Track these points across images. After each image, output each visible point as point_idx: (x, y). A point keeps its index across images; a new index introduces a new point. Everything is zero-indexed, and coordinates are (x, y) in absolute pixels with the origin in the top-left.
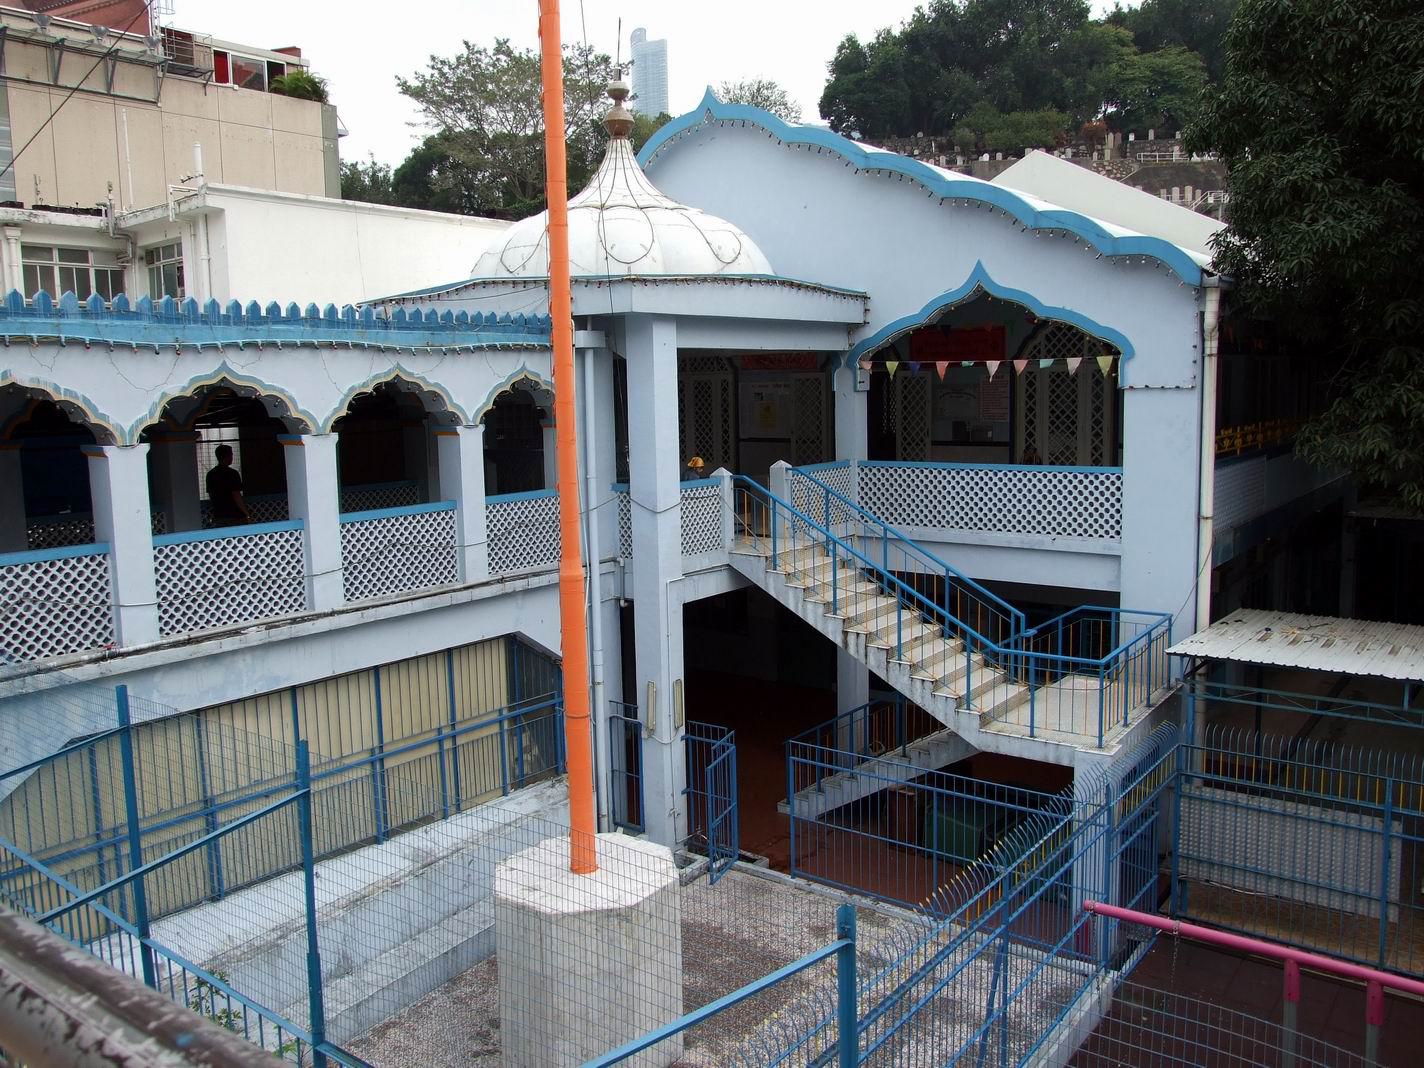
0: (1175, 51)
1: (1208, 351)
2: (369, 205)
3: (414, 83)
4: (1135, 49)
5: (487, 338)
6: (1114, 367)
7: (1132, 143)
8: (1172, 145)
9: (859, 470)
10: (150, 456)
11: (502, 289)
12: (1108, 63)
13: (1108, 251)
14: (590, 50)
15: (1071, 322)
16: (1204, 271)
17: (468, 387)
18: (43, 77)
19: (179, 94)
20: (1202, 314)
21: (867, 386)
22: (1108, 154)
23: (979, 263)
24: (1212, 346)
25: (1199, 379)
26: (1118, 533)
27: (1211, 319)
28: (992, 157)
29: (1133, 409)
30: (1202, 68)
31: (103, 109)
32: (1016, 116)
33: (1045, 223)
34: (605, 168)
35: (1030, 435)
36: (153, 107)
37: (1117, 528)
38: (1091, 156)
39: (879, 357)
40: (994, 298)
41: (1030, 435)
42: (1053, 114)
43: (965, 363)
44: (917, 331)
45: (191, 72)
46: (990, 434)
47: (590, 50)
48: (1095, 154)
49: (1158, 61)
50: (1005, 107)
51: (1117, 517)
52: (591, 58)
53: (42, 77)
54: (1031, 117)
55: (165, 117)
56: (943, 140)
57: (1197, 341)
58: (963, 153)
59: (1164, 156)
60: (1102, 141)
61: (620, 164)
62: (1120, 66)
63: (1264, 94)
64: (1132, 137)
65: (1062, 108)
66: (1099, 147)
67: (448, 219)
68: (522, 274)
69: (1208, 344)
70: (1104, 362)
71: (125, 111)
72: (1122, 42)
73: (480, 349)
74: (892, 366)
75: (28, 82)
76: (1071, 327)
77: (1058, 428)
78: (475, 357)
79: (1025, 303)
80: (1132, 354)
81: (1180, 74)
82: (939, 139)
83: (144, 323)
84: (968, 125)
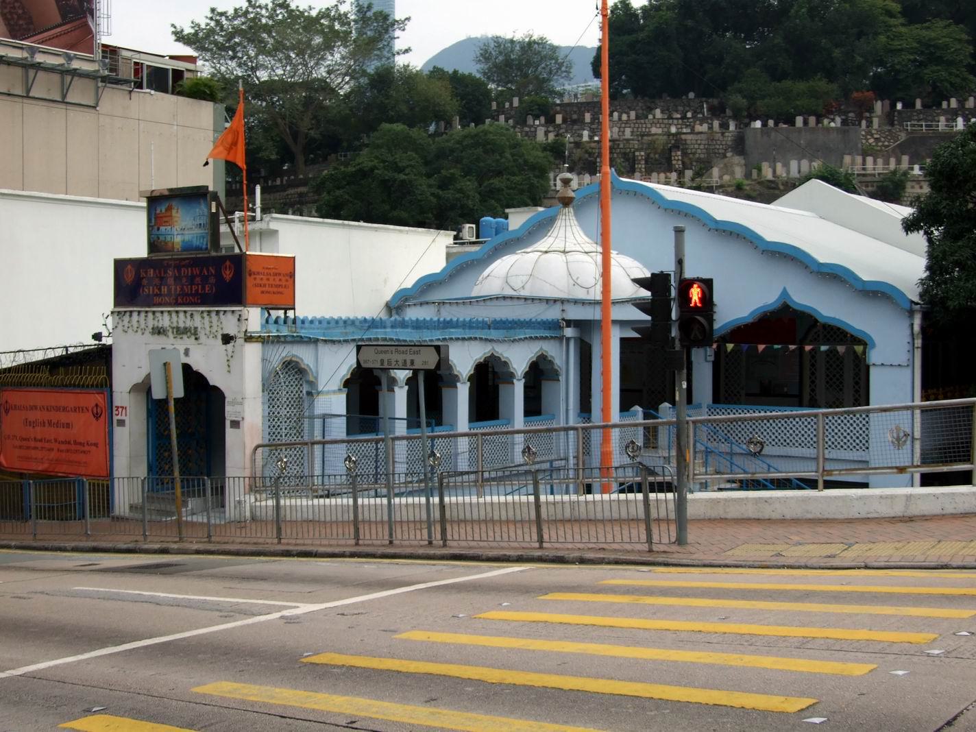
0: (941, 23)
1: (916, 345)
2: (340, 222)
3: (188, 30)
4: (902, 20)
5: (529, 333)
6: (864, 352)
7: (899, 111)
8: (938, 115)
9: (707, 410)
10: (408, 391)
11: (515, 302)
12: (876, 34)
13: (860, 287)
14: (369, 7)
15: (839, 325)
16: (912, 302)
17: (519, 358)
18: (19, 91)
19: (113, 100)
20: (912, 325)
21: (712, 359)
22: (876, 121)
23: (785, 288)
24: (918, 342)
25: (911, 360)
26: (867, 448)
27: (917, 328)
28: (765, 125)
29: (875, 376)
30: (968, 42)
31: (58, 112)
32: (787, 84)
33: (824, 270)
34: (559, 225)
35: (813, 390)
36: (93, 111)
37: (867, 445)
38: (860, 124)
39: (724, 339)
40: (794, 310)
41: (813, 390)
42: (821, 84)
43: (776, 346)
44: (746, 326)
45: (118, 82)
46: (786, 389)
47: (369, 7)
48: (864, 123)
49: (924, 33)
50: (777, 75)
51: (867, 445)
52: (369, 14)
53: (19, 91)
54: (801, 86)
55: (102, 118)
56: (715, 102)
57: (909, 339)
58: (735, 117)
59: (931, 126)
60: (871, 109)
61: (568, 223)
62: (888, 37)
63: (944, 207)
64: (899, 106)
65: (830, 76)
66: (867, 114)
67: (400, 231)
68: (524, 293)
69: (916, 341)
70: (859, 349)
71: (74, 113)
72: (890, 14)
73: (526, 338)
74: (730, 346)
75: (9, 95)
76: (839, 329)
77: (831, 386)
78: (522, 343)
79: (813, 314)
80: (874, 346)
81: (946, 46)
82: (710, 100)
83: (409, 330)
84: (740, 91)
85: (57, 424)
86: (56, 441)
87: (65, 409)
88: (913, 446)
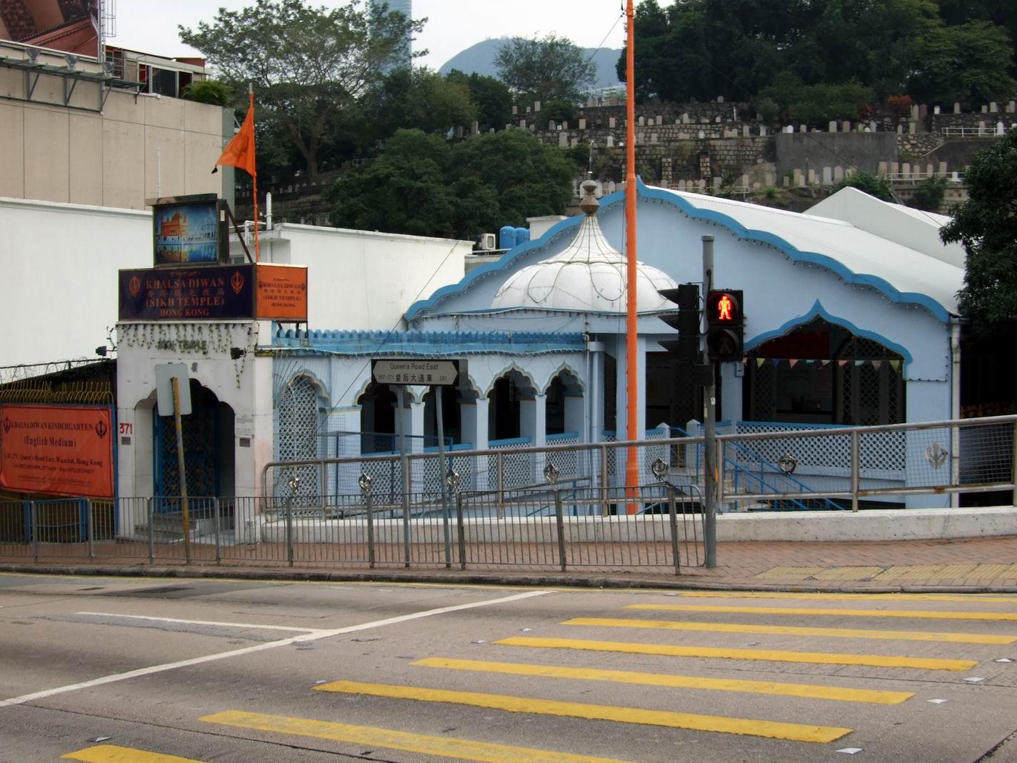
0: (981, 24)
1: (954, 360)
2: (355, 231)
3: (196, 31)
4: (939, 21)
5: (551, 347)
6: (901, 367)
7: (937, 116)
8: (978, 120)
9: (737, 427)
10: (425, 408)
11: (537, 315)
12: (913, 35)
13: (896, 299)
14: (385, 7)
15: (874, 339)
16: (951, 315)
17: (540, 374)
18: (19, 95)
19: (118, 104)
20: (951, 338)
21: (742, 374)
22: (912, 126)
23: (818, 301)
24: (957, 357)
25: (949, 375)
26: (904, 467)
27: (955, 342)
28: (797, 130)
29: (912, 392)
30: (1009, 44)
31: (61, 116)
32: (820, 87)
33: (859, 281)
34: (582, 234)
35: (847, 407)
36: (97, 116)
37: (903, 464)
38: (896, 130)
39: (754, 354)
40: (827, 323)
41: (847, 407)
42: (856, 88)
43: (809, 361)
44: (778, 340)
45: (123, 85)
46: (819, 406)
47: (385, 7)
48: (900, 128)
49: (963, 34)
50: (810, 78)
51: (903, 464)
52: (385, 15)
53: (19, 95)
54: (835, 90)
55: (106, 123)
56: (745, 106)
57: (947, 354)
58: (766, 122)
59: (970, 131)
60: (907, 114)
61: (592, 233)
62: (925, 39)
63: (984, 216)
64: (937, 111)
65: (865, 79)
66: (904, 119)
67: (417, 241)
68: (546, 306)
69: (954, 356)
70: (895, 363)
71: (77, 118)
72: (927, 14)
73: (548, 353)
74: (761, 361)
75: (9, 99)
76: (874, 343)
77: (866, 402)
78: (544, 358)
79: (847, 327)
80: (910, 360)
81: (986, 48)
82: (740, 105)
83: (427, 344)
84: (771, 95)
85: (60, 442)
86: (58, 459)
87: (67, 426)
88: (951, 465)
